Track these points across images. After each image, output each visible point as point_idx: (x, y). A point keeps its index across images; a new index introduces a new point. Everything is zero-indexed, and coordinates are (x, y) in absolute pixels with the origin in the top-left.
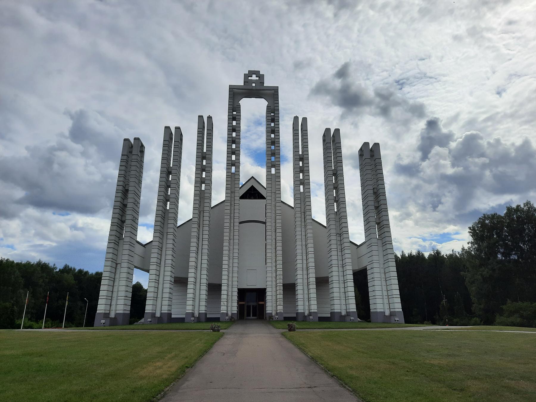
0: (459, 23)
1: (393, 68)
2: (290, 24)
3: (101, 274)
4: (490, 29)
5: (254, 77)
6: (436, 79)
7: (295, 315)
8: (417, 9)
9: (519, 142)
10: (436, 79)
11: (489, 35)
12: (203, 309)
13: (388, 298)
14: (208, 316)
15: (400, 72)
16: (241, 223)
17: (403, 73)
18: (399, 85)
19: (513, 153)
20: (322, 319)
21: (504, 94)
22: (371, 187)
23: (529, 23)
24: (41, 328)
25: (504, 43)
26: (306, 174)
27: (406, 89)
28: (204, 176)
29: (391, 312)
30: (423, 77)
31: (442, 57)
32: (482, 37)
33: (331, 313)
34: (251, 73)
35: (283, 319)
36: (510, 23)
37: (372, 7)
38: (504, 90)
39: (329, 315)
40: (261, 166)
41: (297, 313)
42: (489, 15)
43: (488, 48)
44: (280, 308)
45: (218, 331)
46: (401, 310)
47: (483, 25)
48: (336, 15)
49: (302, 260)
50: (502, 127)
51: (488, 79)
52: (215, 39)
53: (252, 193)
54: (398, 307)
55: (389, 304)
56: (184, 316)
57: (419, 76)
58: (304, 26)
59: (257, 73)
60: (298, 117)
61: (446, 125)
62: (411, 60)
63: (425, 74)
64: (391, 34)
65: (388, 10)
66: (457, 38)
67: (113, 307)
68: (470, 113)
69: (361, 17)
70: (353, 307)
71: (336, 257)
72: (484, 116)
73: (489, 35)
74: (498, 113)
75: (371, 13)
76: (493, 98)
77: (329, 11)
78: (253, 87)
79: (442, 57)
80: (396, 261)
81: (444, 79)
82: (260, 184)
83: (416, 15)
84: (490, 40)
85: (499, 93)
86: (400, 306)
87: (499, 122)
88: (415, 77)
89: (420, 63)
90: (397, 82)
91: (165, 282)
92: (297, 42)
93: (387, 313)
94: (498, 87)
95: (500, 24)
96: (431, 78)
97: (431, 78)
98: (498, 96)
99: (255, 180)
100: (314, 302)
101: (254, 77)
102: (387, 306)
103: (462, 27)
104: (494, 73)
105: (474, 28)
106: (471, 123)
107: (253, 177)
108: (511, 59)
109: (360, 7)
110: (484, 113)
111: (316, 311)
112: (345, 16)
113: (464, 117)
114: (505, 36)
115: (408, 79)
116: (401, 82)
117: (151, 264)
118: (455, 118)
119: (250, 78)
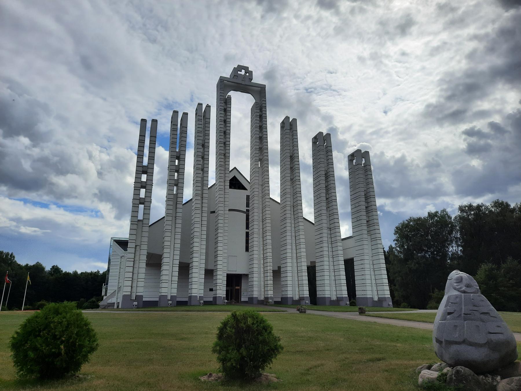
0: (365, 46)
1: (306, 76)
2: (218, 16)
3: (315, 262)
4: (388, 56)
5: (243, 72)
6: (338, 92)
7: (186, 299)
8: (333, 26)
9: (398, 155)
10: (338, 92)
11: (386, 61)
12: (174, 292)
13: (377, 286)
14: (178, 299)
15: (311, 81)
16: (230, 210)
17: (312, 83)
18: (308, 92)
19: (392, 163)
20: (206, 303)
21: (389, 113)
22: (363, 189)
23: (417, 57)
24: (20, 309)
25: (396, 70)
26: (181, 162)
27: (314, 96)
28: (177, 161)
29: (379, 298)
30: (329, 88)
31: (346, 73)
32: (381, 62)
33: (282, 298)
34: (240, 68)
35: (273, 303)
36: (404, 54)
37: (296, 17)
38: (390, 110)
39: (211, 299)
40: (166, 150)
41: (190, 297)
42: (389, 44)
43: (384, 72)
44: (174, 292)
45: (305, 312)
46: (389, 296)
47: (383, 52)
48: (263, 17)
49: (292, 249)
50: (383, 141)
51: (379, 99)
52: (138, 18)
53: (236, 183)
54: (387, 293)
55: (377, 291)
56: (157, 299)
57: (325, 86)
58: (232, 21)
59: (246, 69)
60: (289, 118)
61: (343, 133)
62: (321, 71)
63: (331, 86)
64: (308, 44)
65: (310, 22)
66: (361, 59)
67: (134, 289)
68: (361, 125)
69: (285, 24)
70: (306, 293)
71: (326, 249)
72: (370, 131)
73: (386, 61)
74: (381, 129)
75: (294, 21)
76: (380, 115)
77: (257, 11)
78: (239, 81)
79: (346, 73)
80: (385, 255)
81: (344, 93)
82: (242, 175)
83: (331, 31)
84: (386, 65)
85: (385, 112)
86: (308, 293)
87: (382, 136)
88: (322, 88)
89: (329, 75)
90: (306, 90)
91: (174, 265)
92: (222, 35)
93: (376, 299)
94: (386, 107)
95: (395, 53)
96: (334, 90)
97: (334, 90)
98: (384, 114)
99: (238, 170)
100: (270, 288)
101: (243, 72)
102: (375, 293)
103: (365, 49)
104: (385, 94)
105: (376, 53)
106: (360, 134)
107: (235, 168)
108: (399, 85)
109: (285, 15)
110: (371, 127)
111: (175, 295)
112: (271, 19)
113: (356, 129)
114: (399, 65)
115: (315, 89)
116: (310, 90)
117: (165, 247)
118: (349, 128)
119: (239, 72)
